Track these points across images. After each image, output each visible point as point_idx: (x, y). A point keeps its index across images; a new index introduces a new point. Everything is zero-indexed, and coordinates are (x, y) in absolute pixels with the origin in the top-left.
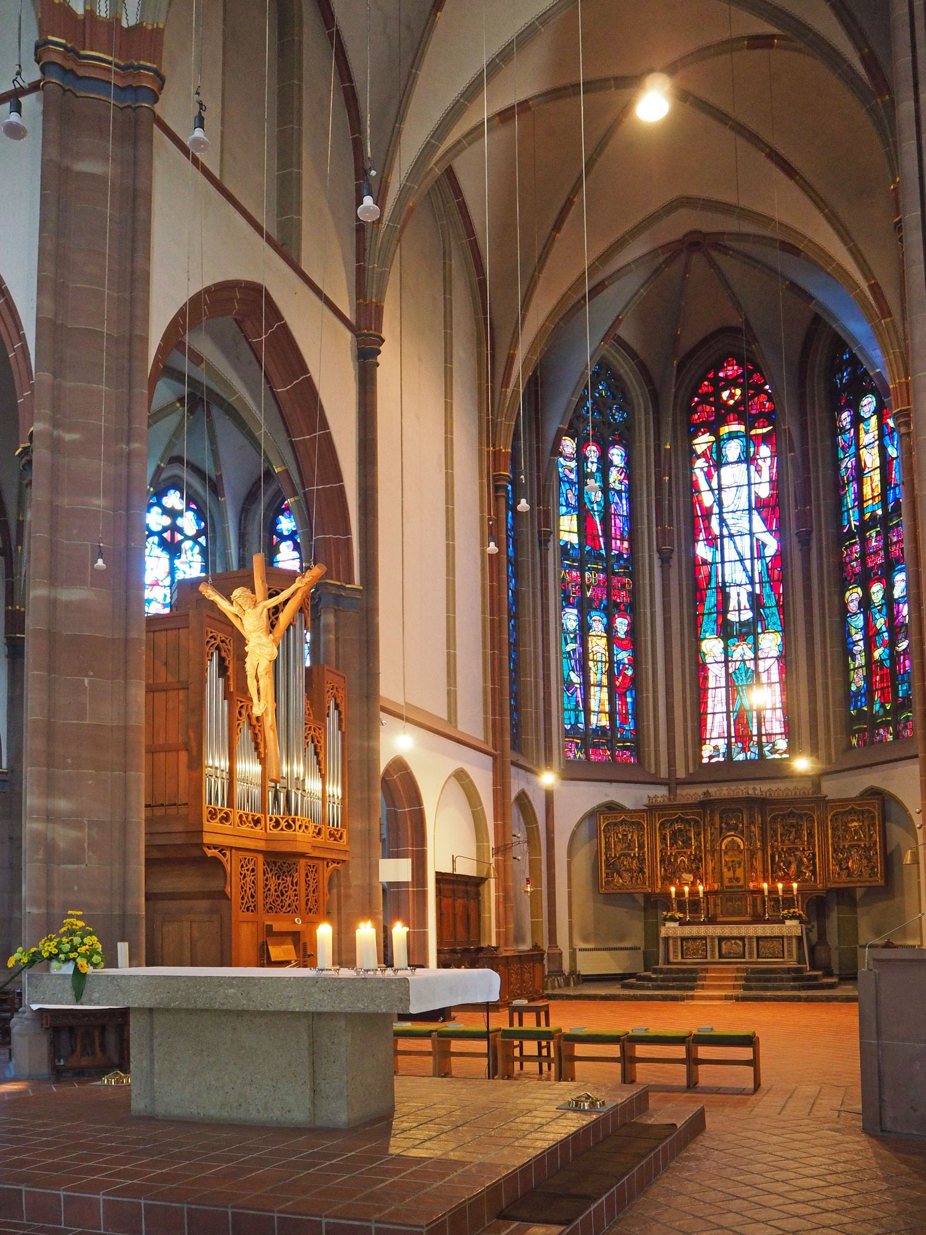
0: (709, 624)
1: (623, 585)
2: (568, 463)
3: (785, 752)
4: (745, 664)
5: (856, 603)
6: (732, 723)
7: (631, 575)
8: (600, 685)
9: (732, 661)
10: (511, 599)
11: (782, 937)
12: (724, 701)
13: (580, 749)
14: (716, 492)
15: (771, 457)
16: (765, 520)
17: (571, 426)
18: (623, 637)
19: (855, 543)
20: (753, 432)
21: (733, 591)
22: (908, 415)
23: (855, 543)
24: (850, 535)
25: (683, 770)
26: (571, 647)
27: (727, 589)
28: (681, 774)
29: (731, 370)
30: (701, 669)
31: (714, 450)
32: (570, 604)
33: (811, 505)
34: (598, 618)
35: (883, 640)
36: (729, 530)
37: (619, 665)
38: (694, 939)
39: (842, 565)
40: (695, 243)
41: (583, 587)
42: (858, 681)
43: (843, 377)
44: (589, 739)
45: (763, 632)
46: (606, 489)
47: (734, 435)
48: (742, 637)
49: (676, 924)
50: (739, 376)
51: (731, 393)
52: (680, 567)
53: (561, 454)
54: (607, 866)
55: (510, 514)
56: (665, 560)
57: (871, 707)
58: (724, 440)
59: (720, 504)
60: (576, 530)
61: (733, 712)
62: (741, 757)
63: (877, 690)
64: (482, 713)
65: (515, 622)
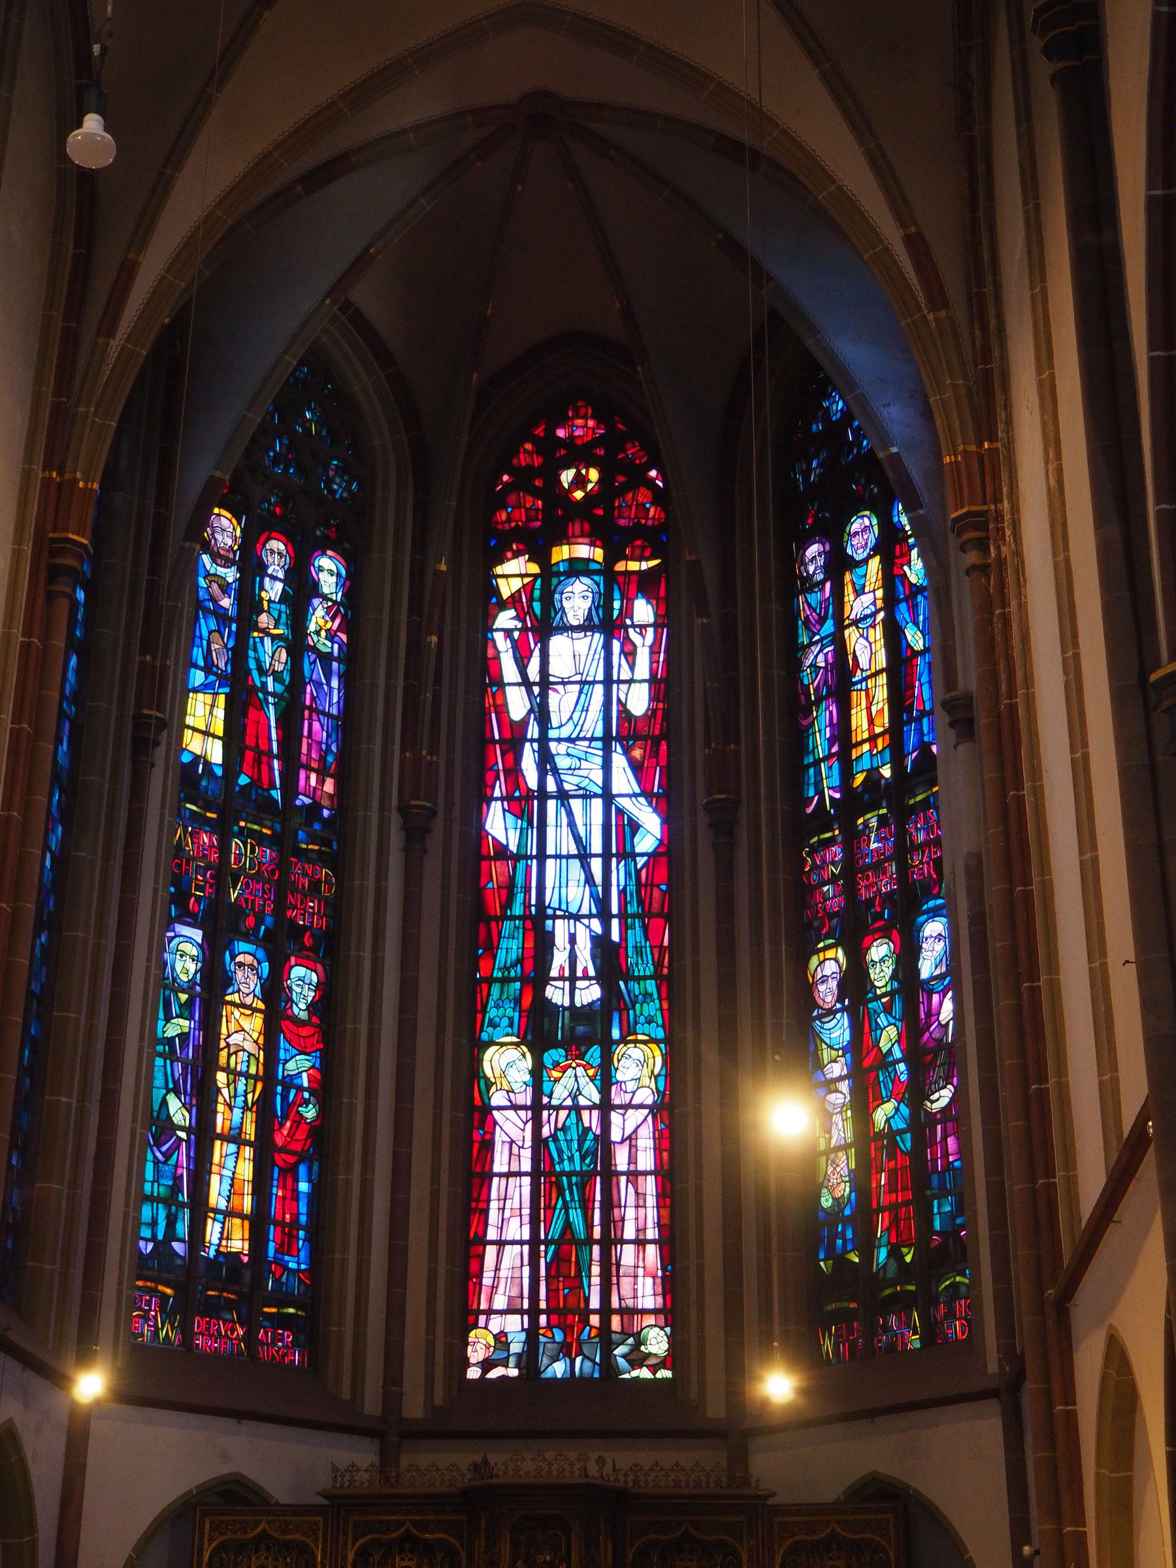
0: (501, 1010)
1: (315, 885)
2: (221, 571)
3: (663, 1364)
4: (579, 1118)
5: (833, 984)
6: (543, 1272)
7: (334, 861)
9: (549, 1107)
10: (48, 878)
12: (526, 1212)
13: (168, 1316)
14: (536, 690)
15: (655, 625)
16: (636, 767)
17: (236, 483)
18: (304, 1015)
20: (620, 567)
21: (561, 930)
22: (983, 526)
24: (822, 820)
25: (421, 1400)
26: (177, 1027)
27: (549, 923)
28: (414, 1407)
29: (583, 427)
30: (480, 1117)
31: (537, 594)
32: (188, 914)
33: (738, 743)
34: (249, 959)
35: (896, 1080)
36: (559, 783)
37: (286, 1091)
39: (802, 892)
40: (543, 118)
41: (223, 875)
43: (810, 469)
44: (199, 1284)
45: (623, 1040)
46: (297, 644)
47: (580, 566)
48: (575, 1048)
51: (578, 474)
52: (446, 853)
53: (207, 547)
55: (73, 661)
57: (868, 1255)
58: (558, 574)
59: (542, 713)
60: (220, 731)
61: (547, 1243)
62: (559, 1369)
64: (10, 537)
65: (50, 939)
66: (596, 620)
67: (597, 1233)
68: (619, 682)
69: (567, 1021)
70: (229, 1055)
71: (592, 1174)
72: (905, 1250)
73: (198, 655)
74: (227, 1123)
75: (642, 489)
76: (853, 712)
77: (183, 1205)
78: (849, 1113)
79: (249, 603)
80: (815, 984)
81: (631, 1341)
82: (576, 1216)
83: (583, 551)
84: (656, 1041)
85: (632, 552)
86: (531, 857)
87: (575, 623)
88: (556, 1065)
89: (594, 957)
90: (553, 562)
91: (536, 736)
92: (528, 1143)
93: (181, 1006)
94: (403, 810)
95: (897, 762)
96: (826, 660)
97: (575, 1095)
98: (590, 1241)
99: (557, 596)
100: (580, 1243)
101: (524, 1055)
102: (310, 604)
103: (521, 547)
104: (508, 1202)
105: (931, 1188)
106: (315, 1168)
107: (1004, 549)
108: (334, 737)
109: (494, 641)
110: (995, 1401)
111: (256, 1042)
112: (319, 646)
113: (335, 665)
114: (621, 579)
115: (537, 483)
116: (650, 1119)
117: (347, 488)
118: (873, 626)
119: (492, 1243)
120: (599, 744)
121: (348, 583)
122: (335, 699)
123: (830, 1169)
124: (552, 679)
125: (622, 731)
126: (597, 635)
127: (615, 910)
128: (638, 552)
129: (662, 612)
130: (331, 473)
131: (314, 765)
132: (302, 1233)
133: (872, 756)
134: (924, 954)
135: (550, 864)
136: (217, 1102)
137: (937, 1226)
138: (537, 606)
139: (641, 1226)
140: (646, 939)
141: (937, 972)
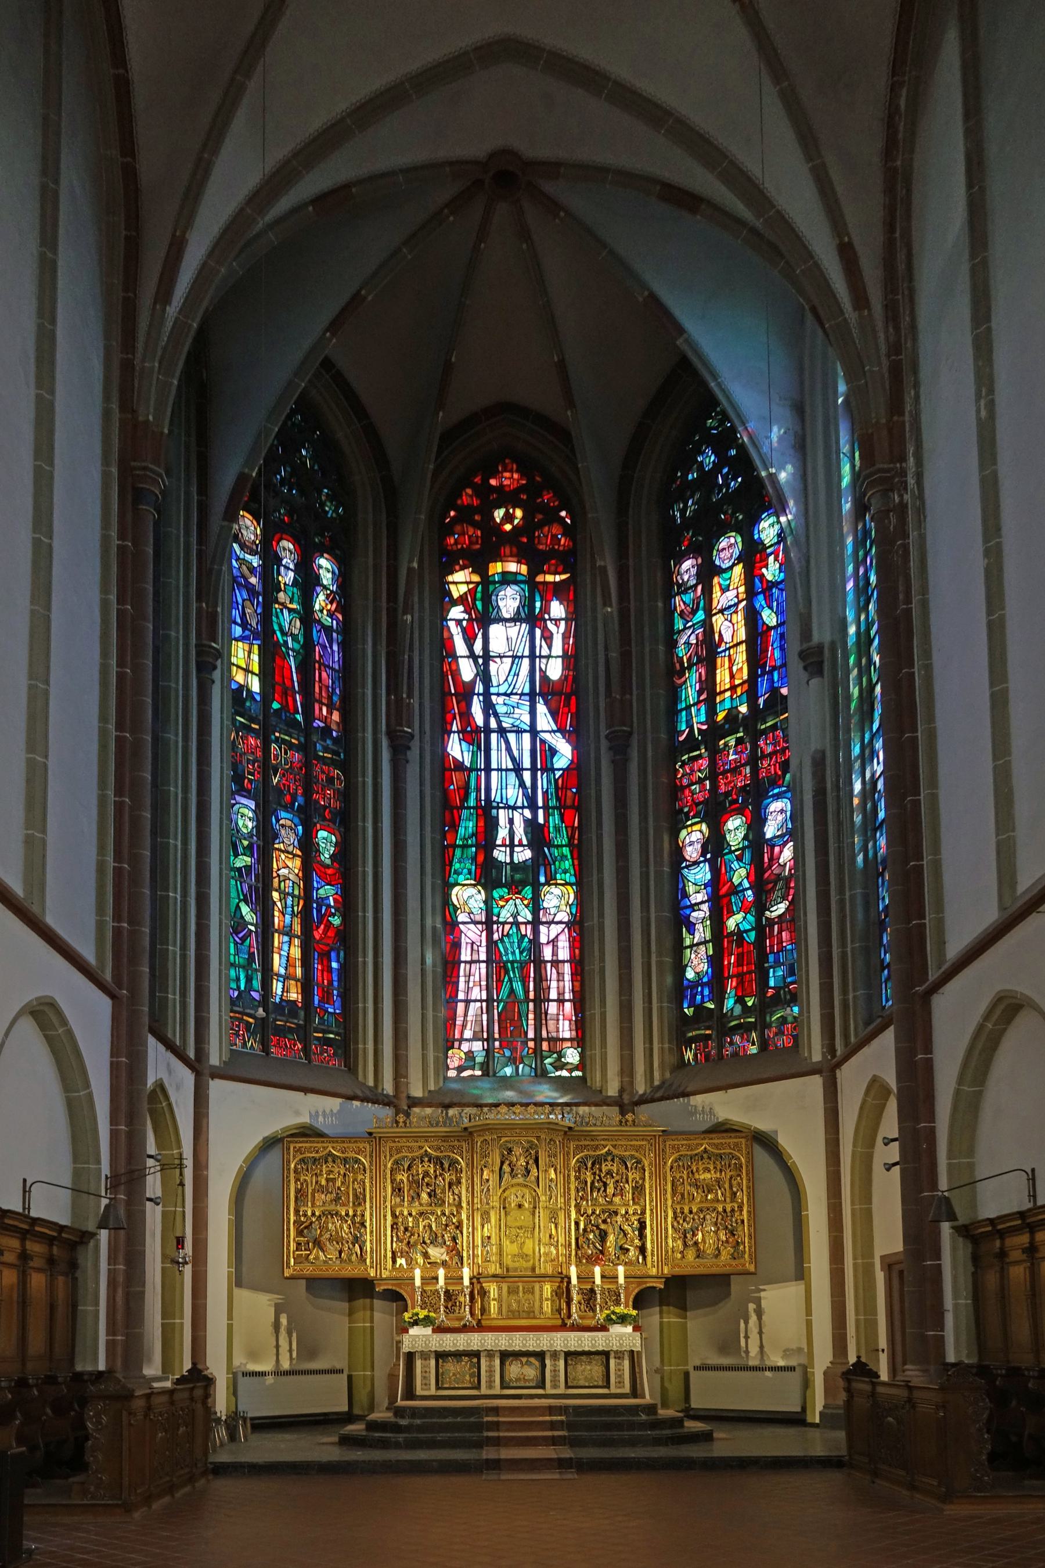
0: (462, 866)
2: (248, 557)
3: (577, 1068)
4: (518, 929)
8: (288, 932)
11: (606, 1354)
12: (484, 983)
14: (480, 661)
16: (554, 714)
18: (328, 862)
19: (700, 756)
20: (540, 578)
21: (503, 816)
23: (700, 756)
27: (494, 812)
29: (509, 479)
31: (479, 595)
33: (631, 694)
34: (289, 823)
36: (499, 722)
38: (458, 1355)
39: (676, 790)
40: (504, 177)
41: (267, 768)
42: (697, 965)
43: (686, 507)
45: (548, 883)
46: (307, 617)
47: (510, 578)
48: (515, 887)
49: (428, 1331)
50: (521, 489)
53: (236, 538)
54: (300, 1233)
56: (399, 747)
57: (720, 1003)
58: (495, 582)
59: (485, 676)
60: (256, 670)
63: (729, 977)
66: (523, 615)
67: (532, 995)
68: (541, 657)
69: (508, 872)
70: (280, 882)
71: (527, 963)
72: (747, 999)
73: (236, 614)
74: (282, 923)
75: (555, 525)
76: (718, 671)
77: (256, 970)
78: (708, 922)
79: (270, 586)
80: (684, 846)
81: (555, 1055)
82: (518, 987)
83: (512, 567)
84: (571, 884)
85: (549, 568)
86: (481, 770)
87: (507, 616)
88: (502, 898)
89: (526, 833)
90: (490, 573)
91: (481, 691)
92: (484, 943)
93: (244, 848)
94: (390, 734)
95: (752, 696)
96: (697, 638)
97: (515, 916)
98: (527, 1000)
99: (494, 597)
100: (520, 1002)
101: (479, 892)
102: (314, 589)
103: (466, 562)
104: (472, 978)
105: (768, 962)
106: (342, 954)
107: (905, 497)
108: (337, 683)
109: (448, 628)
110: (817, 1077)
111: (297, 875)
112: (323, 621)
113: (335, 635)
114: (541, 587)
115: (476, 517)
116: (566, 930)
117: (336, 511)
118: (736, 612)
119: (461, 1001)
120: (527, 698)
121: (340, 579)
122: (336, 659)
123: (693, 956)
124: (491, 654)
125: (540, 690)
126: (524, 625)
127: (540, 804)
128: (553, 568)
129: (571, 609)
130: (323, 498)
131: (325, 701)
132: (335, 992)
133: (732, 699)
134: (769, 823)
135: (494, 774)
136: (273, 910)
137: (772, 983)
138: (479, 604)
139: (561, 991)
140: (563, 821)
141: (779, 833)
